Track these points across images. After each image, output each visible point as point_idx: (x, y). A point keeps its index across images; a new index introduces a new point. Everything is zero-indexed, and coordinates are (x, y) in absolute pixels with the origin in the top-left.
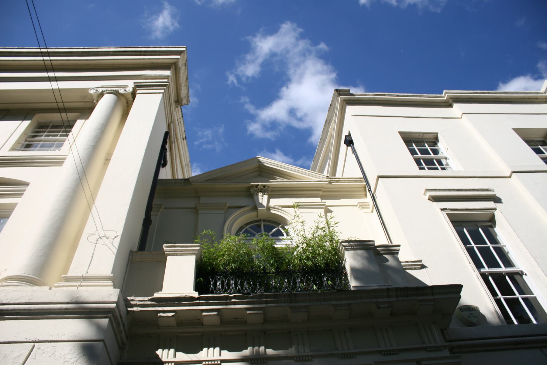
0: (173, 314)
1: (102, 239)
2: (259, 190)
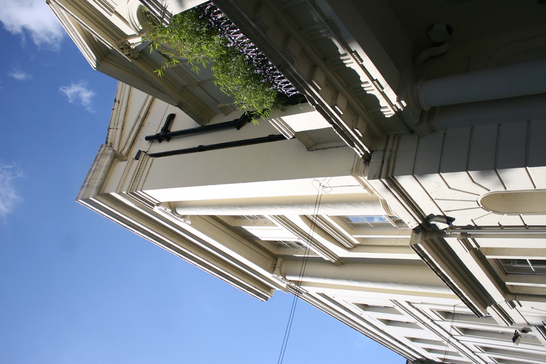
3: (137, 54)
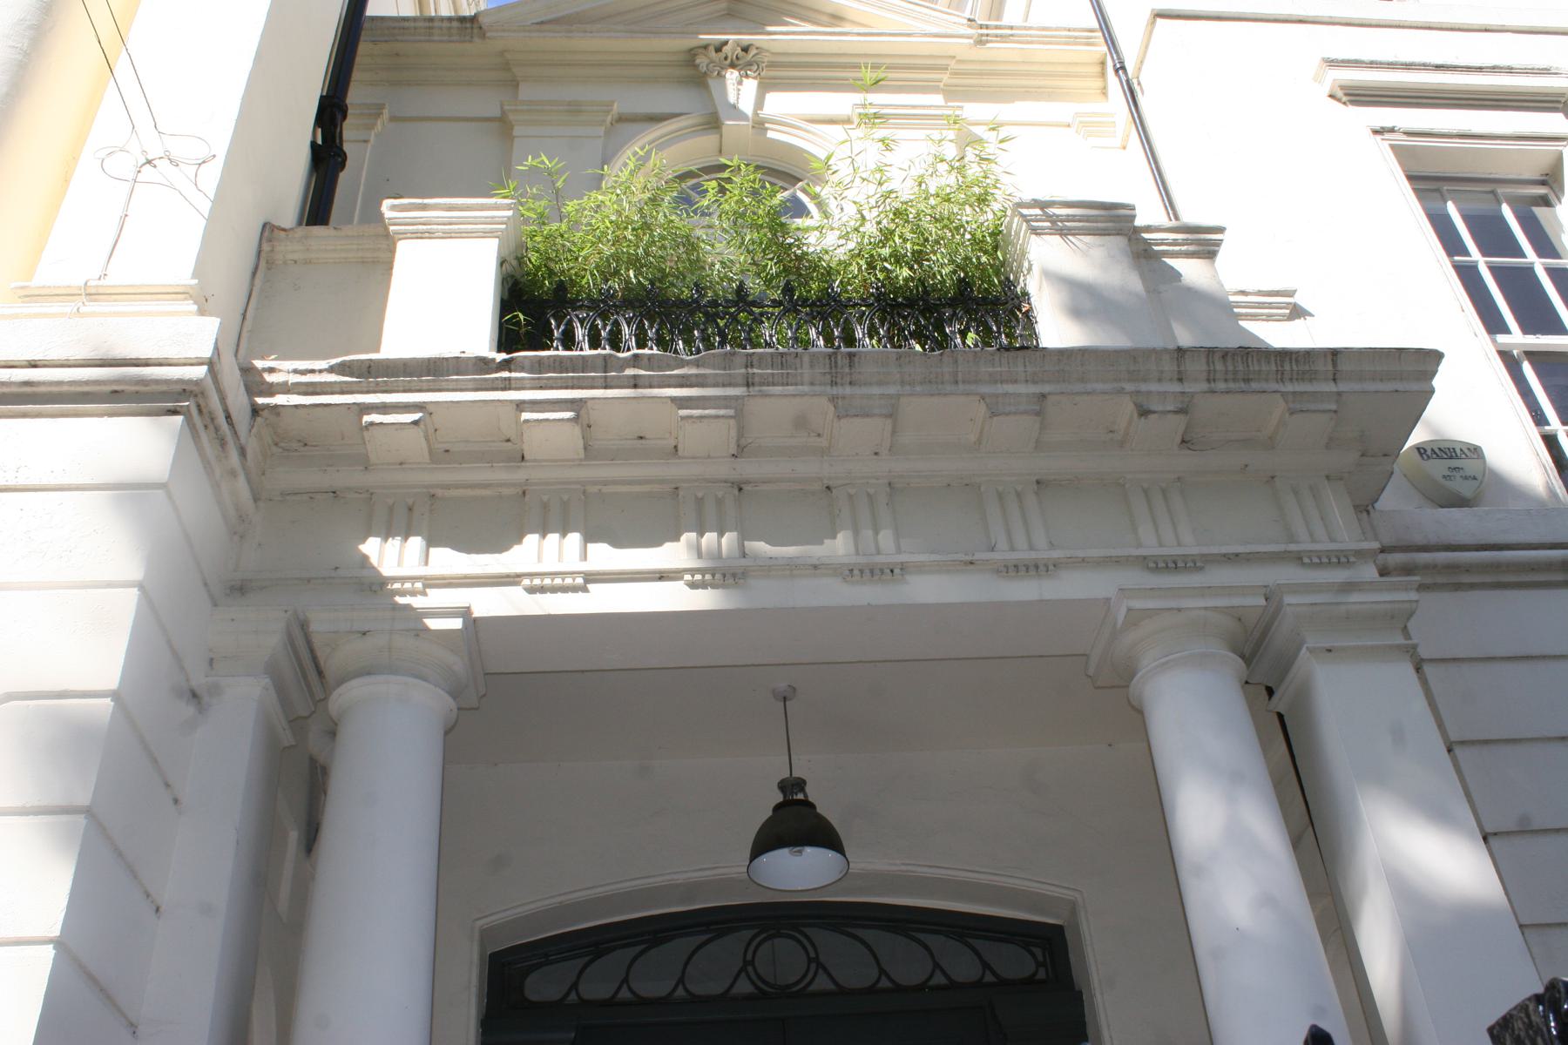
0: (416, 416)
1: (155, 166)
2: (729, 60)
3: (705, 68)
